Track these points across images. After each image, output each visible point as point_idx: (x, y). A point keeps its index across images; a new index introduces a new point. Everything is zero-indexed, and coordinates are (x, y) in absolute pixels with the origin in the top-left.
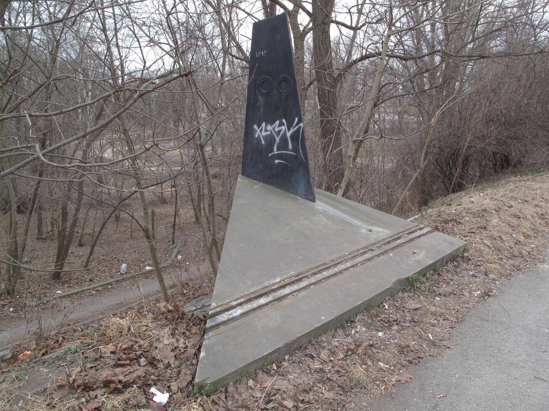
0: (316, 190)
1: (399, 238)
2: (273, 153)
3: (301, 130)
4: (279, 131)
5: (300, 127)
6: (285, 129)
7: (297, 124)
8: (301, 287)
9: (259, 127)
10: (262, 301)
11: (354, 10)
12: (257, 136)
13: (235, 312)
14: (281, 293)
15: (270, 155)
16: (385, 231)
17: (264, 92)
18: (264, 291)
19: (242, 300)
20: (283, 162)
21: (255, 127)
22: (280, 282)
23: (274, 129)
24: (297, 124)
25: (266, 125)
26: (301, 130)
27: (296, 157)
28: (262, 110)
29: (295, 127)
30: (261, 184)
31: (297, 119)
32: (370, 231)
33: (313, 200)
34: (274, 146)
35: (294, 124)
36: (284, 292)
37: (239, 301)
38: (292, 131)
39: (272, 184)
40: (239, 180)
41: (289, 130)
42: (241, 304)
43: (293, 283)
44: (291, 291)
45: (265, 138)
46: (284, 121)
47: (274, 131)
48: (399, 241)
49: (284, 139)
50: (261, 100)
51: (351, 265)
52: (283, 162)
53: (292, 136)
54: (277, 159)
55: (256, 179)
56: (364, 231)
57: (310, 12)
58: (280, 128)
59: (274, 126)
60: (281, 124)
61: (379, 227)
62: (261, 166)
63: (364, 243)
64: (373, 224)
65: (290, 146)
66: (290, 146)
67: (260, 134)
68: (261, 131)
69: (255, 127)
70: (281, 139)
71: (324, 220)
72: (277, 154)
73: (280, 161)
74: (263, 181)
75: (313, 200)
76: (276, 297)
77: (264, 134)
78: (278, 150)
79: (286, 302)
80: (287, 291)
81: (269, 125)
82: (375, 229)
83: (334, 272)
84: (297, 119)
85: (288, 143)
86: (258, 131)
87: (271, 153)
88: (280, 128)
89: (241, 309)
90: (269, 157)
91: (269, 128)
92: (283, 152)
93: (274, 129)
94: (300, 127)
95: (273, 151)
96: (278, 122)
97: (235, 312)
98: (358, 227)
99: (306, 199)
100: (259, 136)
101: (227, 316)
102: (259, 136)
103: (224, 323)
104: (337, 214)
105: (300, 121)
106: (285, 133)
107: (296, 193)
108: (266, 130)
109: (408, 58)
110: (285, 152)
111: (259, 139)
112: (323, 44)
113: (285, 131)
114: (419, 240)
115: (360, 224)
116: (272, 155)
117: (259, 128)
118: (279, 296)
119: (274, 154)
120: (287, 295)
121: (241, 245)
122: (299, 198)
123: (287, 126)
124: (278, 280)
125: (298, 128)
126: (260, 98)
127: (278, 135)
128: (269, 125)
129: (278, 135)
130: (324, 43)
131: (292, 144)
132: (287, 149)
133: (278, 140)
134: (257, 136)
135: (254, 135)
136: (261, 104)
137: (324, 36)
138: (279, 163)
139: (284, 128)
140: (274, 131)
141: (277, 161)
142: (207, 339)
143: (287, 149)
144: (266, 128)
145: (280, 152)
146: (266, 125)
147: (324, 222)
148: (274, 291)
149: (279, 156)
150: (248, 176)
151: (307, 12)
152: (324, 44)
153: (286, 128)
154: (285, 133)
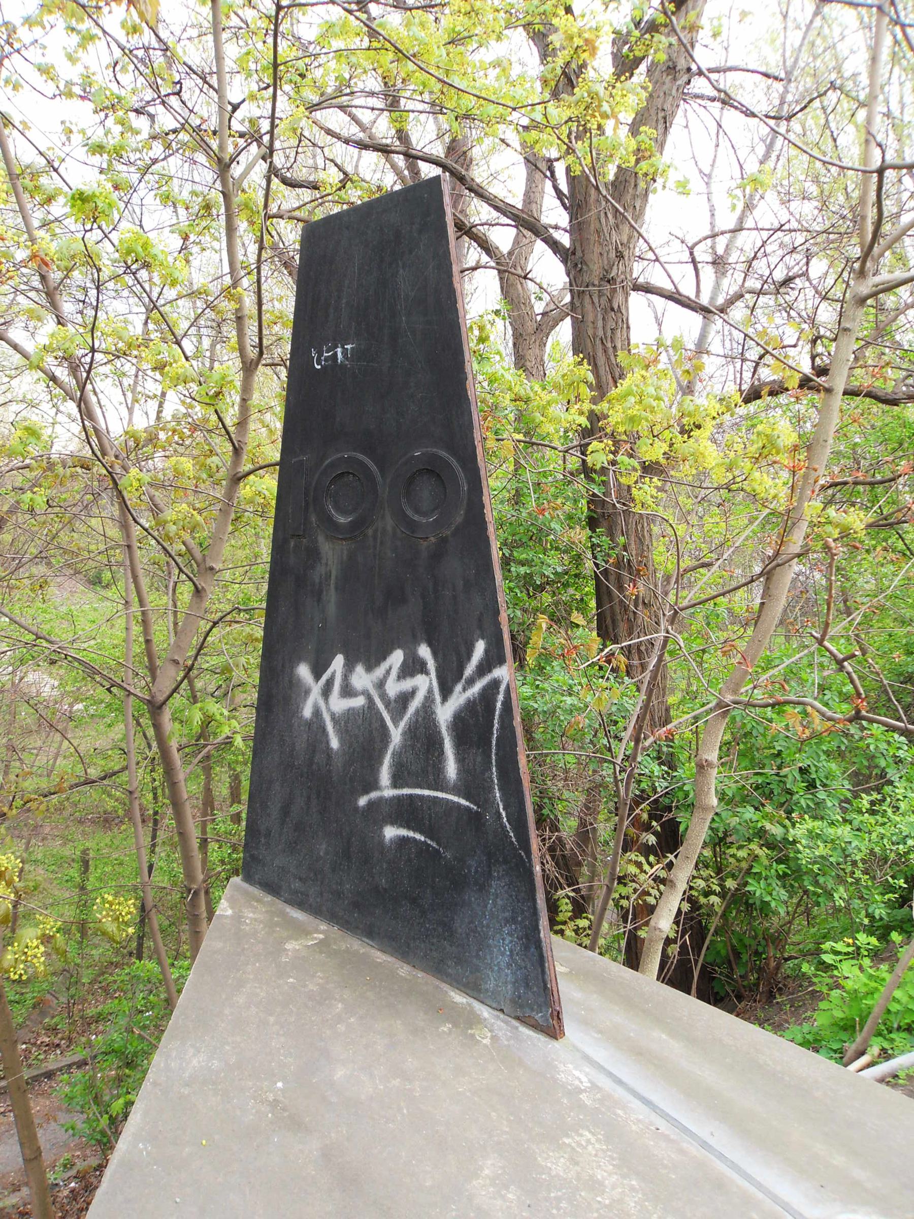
2: (374, 795)
3: (501, 697)
4: (405, 698)
6: (430, 691)
7: (484, 668)
9: (317, 673)
12: (307, 712)
15: (363, 801)
17: (342, 520)
21: (304, 671)
23: (381, 685)
24: (484, 668)
25: (349, 667)
26: (501, 697)
27: (475, 819)
28: (332, 598)
29: (471, 682)
30: (321, 930)
31: (480, 647)
34: (381, 763)
35: (469, 670)
38: (459, 698)
39: (370, 933)
41: (446, 693)
45: (344, 722)
46: (424, 651)
47: (383, 696)
53: (460, 723)
55: (301, 904)
57: (563, 246)
58: (407, 685)
59: (380, 671)
60: (413, 667)
62: (322, 848)
65: (451, 769)
66: (451, 769)
67: (322, 703)
68: (326, 692)
69: (304, 671)
70: (411, 733)
73: (403, 832)
74: (332, 917)
77: (339, 704)
78: (397, 782)
84: (480, 647)
85: (442, 752)
86: (316, 689)
87: (366, 791)
88: (407, 685)
90: (356, 808)
91: (361, 679)
92: (418, 791)
93: (381, 685)
94: (496, 683)
95: (372, 784)
96: (397, 658)
99: (518, 1018)
100: (317, 713)
102: (317, 713)
105: (493, 659)
106: (427, 708)
107: (474, 989)
108: (348, 691)
109: (900, 396)
110: (426, 792)
112: (605, 351)
113: (429, 700)
116: (371, 804)
117: (317, 675)
119: (381, 799)
122: (485, 1012)
123: (439, 677)
130: (609, 345)
131: (460, 759)
132: (438, 783)
133: (396, 735)
134: (307, 712)
135: (298, 709)
136: (328, 575)
137: (611, 324)
138: (403, 842)
139: (424, 683)
140: (383, 696)
141: (391, 832)
143: (438, 783)
144: (346, 678)
146: (349, 667)
150: (272, 888)
154: (427, 708)
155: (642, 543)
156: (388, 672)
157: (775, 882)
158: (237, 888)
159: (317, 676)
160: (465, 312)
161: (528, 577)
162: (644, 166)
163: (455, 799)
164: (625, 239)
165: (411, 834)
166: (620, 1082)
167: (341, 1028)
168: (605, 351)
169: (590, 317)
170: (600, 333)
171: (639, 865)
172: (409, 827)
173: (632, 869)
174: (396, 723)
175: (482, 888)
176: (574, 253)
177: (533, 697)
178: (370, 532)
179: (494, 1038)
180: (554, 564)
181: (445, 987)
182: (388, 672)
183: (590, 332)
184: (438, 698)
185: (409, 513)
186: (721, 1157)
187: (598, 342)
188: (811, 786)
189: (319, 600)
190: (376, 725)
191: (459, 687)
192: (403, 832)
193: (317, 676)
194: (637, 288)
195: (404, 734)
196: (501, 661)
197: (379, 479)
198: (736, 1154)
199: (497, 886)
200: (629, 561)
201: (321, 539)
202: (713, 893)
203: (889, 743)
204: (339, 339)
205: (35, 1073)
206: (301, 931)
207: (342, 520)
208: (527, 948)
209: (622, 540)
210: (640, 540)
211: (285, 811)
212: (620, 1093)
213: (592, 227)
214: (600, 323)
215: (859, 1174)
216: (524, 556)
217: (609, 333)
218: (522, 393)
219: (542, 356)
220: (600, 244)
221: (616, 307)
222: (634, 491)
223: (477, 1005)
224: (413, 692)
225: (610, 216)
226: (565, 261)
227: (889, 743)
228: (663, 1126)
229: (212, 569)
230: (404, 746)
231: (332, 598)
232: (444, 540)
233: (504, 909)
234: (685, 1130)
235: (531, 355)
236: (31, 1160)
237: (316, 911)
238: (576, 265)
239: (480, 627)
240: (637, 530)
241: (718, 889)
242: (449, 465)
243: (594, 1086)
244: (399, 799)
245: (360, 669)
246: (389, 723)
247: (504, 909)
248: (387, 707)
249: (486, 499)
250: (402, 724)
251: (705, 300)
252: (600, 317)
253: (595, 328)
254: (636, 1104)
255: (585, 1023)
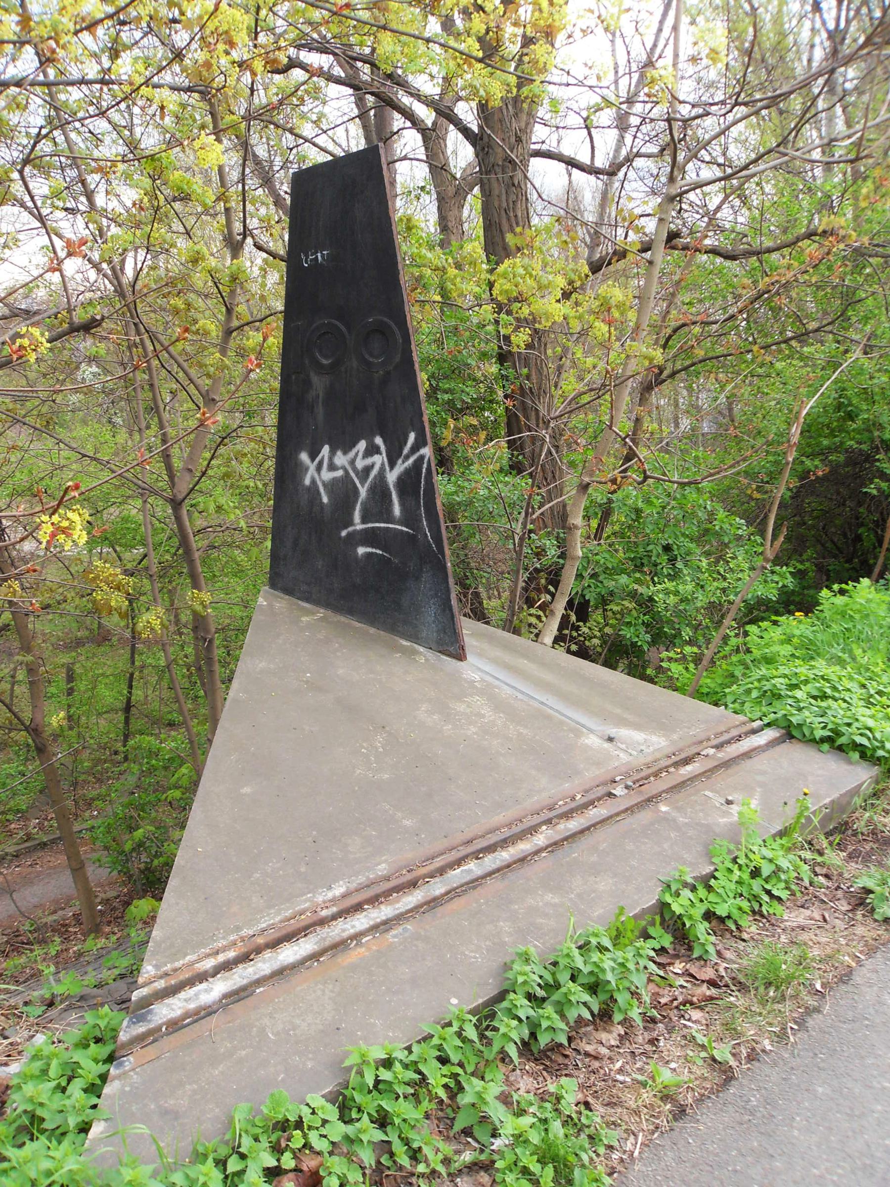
0: (468, 627)
1: (687, 761)
2: (351, 529)
3: (425, 466)
4: (368, 469)
5: (422, 458)
6: (383, 464)
7: (415, 448)
8: (403, 910)
9: (313, 458)
10: (289, 954)
11: (606, 117)
12: (307, 482)
13: (206, 991)
14: (343, 931)
15: (344, 533)
16: (654, 739)
17: (325, 362)
18: (294, 924)
19: (231, 954)
20: (379, 552)
21: (304, 457)
22: (344, 896)
23: (352, 462)
24: (415, 448)
25: (333, 453)
26: (425, 466)
27: (412, 539)
28: (320, 411)
29: (407, 457)
30: (321, 613)
31: (412, 437)
32: (610, 739)
33: (460, 655)
34: (354, 509)
35: (406, 451)
36: (353, 927)
37: (221, 958)
38: (401, 467)
39: (350, 612)
40: (262, 601)
41: (392, 465)
42: (227, 966)
43: (374, 901)
44: (372, 923)
45: (331, 486)
46: (379, 441)
47: (355, 469)
48: (689, 768)
49: (380, 491)
50: (319, 384)
51: (547, 843)
52: (379, 552)
53: (401, 482)
54: (362, 545)
55: (307, 600)
56: (593, 741)
57: (473, 132)
58: (369, 461)
59: (352, 454)
60: (372, 450)
61: (638, 727)
62: (320, 564)
63: (591, 774)
64: (621, 722)
65: (397, 510)
66: (397, 510)
67: (316, 476)
68: (319, 468)
69: (304, 457)
70: (372, 490)
71: (486, 711)
72: (362, 530)
73: (369, 550)
74: (327, 605)
75: (460, 655)
76: (327, 943)
77: (327, 475)
78: (364, 520)
79: (355, 955)
80: (360, 922)
81: (339, 453)
82: (623, 733)
83: (498, 864)
84: (412, 437)
85: (391, 501)
86: (312, 467)
87: (346, 527)
88: (369, 461)
89: (226, 979)
90: (340, 538)
91: (341, 459)
92: (377, 525)
93: (352, 462)
94: (422, 458)
95: (350, 523)
96: (362, 445)
97: (206, 991)
98: (577, 731)
99: (440, 652)
100: (313, 481)
101: (180, 1004)
102: (313, 481)
103: (175, 1026)
104: (523, 693)
105: (421, 442)
106: (381, 475)
107: (415, 638)
108: (332, 467)
109: (737, 252)
110: (382, 525)
111: (313, 488)
112: (509, 219)
113: (382, 470)
114: (748, 764)
115: (584, 719)
116: (349, 534)
117: (313, 459)
118: (338, 939)
119: (355, 531)
120: (357, 936)
121: (246, 790)
122: (421, 649)
123: (387, 456)
124: (339, 890)
125: (415, 461)
126: (315, 379)
127: (363, 481)
128: (339, 453)
129: (363, 481)
130: (512, 214)
131: (402, 504)
132: (390, 519)
133: (363, 492)
134: (307, 482)
135: (302, 479)
136: (318, 396)
137: (513, 197)
138: (369, 555)
139: (378, 460)
140: (355, 469)
141: (361, 550)
142: (118, 1077)
143: (390, 519)
144: (331, 459)
145: (370, 525)
146: (333, 453)
147: (483, 716)
148: (323, 922)
149: (369, 537)
150: (288, 591)
151: (465, 131)
152: (513, 219)
153: (386, 460)
154: (381, 475)
155: (541, 374)
156: (357, 454)
157: (642, 629)
158: (266, 592)
159: (313, 460)
160: (393, 183)
161: (450, 402)
162: (525, 91)
163: (399, 527)
164: (523, 125)
165: (374, 550)
166: (497, 679)
167: (339, 654)
168: (509, 219)
169: (496, 192)
170: (504, 205)
171: (539, 618)
172: (373, 547)
173: (533, 620)
174: (363, 486)
175: (417, 578)
176: (481, 139)
177: (456, 493)
178: (343, 369)
179: (427, 660)
180: (470, 393)
181: (397, 638)
182: (357, 454)
183: (496, 204)
184: (387, 468)
185: (367, 356)
186: (551, 708)
187: (503, 212)
188: (672, 560)
189: (312, 412)
190: (350, 486)
191: (400, 461)
192: (369, 550)
193: (313, 460)
194: (538, 154)
195: (368, 491)
196: (425, 444)
197: (347, 336)
198: (560, 706)
199: (426, 576)
200: (530, 389)
201: (312, 374)
202: (595, 637)
203: (731, 525)
204: (319, 248)
205: (52, 837)
206: (308, 613)
207: (325, 362)
208: (444, 611)
209: (525, 371)
210: (540, 372)
211: (296, 543)
212: (497, 683)
213: (496, 118)
214: (504, 197)
215: (626, 715)
216: (447, 386)
217: (511, 205)
218: (440, 265)
219: (461, 216)
220: (503, 131)
221: (516, 183)
222: (513, 338)
223: (416, 646)
224: (372, 466)
225: (510, 107)
226: (474, 145)
227: (731, 525)
228: (520, 696)
229: (213, 400)
230: (368, 498)
231: (320, 411)
232: (388, 373)
233: (430, 589)
234: (533, 698)
235: (451, 216)
236: (76, 870)
237: (317, 602)
238: (483, 149)
239: (412, 425)
240: (536, 364)
241: (598, 634)
242: (390, 327)
243: (482, 680)
244: (366, 531)
245: (339, 453)
246: (359, 485)
247: (430, 589)
248: (357, 475)
249: (413, 347)
250: (367, 485)
251: (601, 162)
252: (504, 191)
253: (500, 201)
254: (506, 687)
255: (480, 655)
